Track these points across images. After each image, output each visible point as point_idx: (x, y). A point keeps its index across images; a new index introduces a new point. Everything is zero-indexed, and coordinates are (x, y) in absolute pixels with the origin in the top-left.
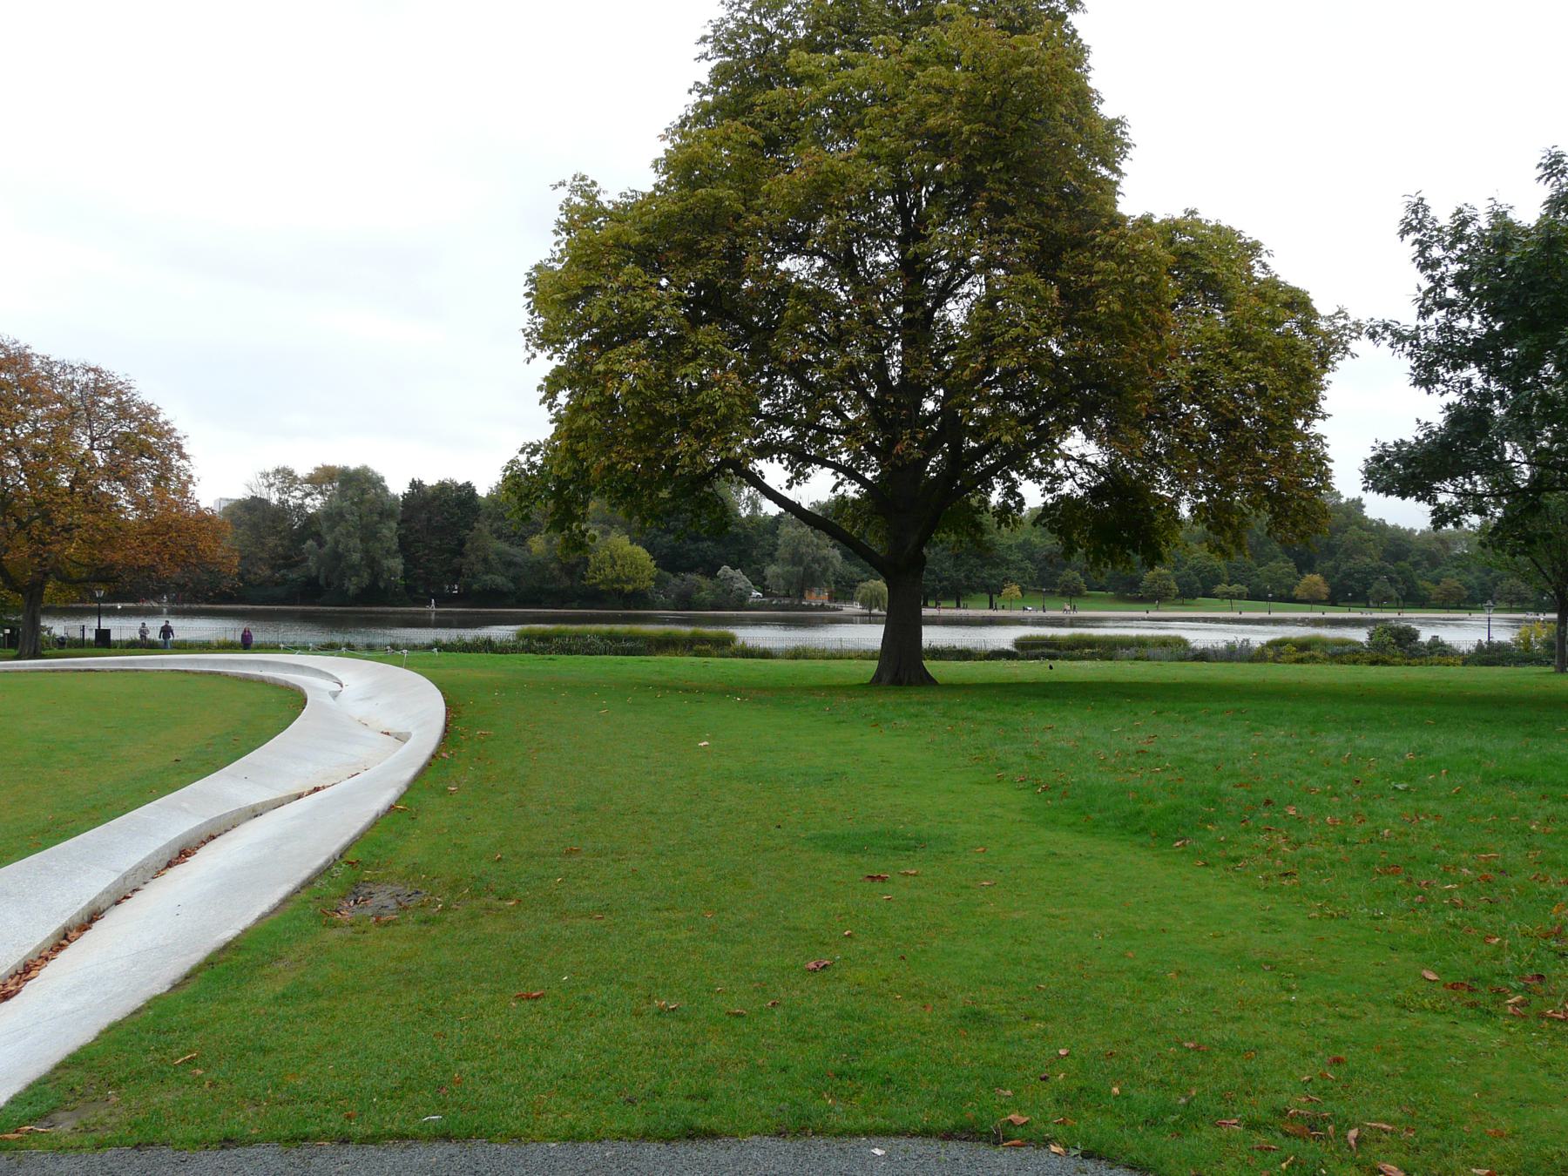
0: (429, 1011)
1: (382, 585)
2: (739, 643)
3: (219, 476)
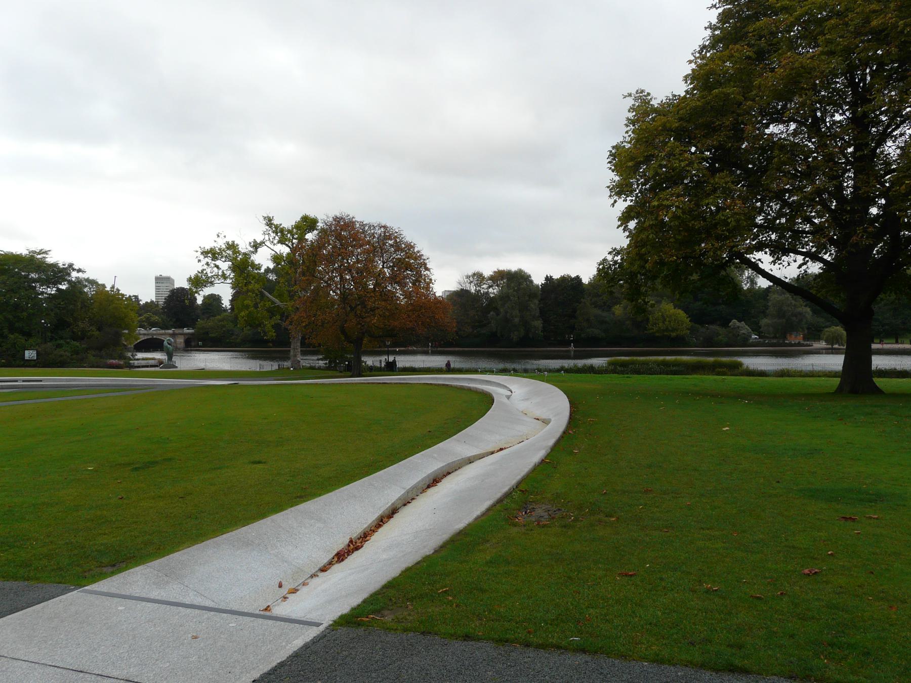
0: (570, 578)
1: (531, 336)
2: (745, 367)
3: (445, 279)
